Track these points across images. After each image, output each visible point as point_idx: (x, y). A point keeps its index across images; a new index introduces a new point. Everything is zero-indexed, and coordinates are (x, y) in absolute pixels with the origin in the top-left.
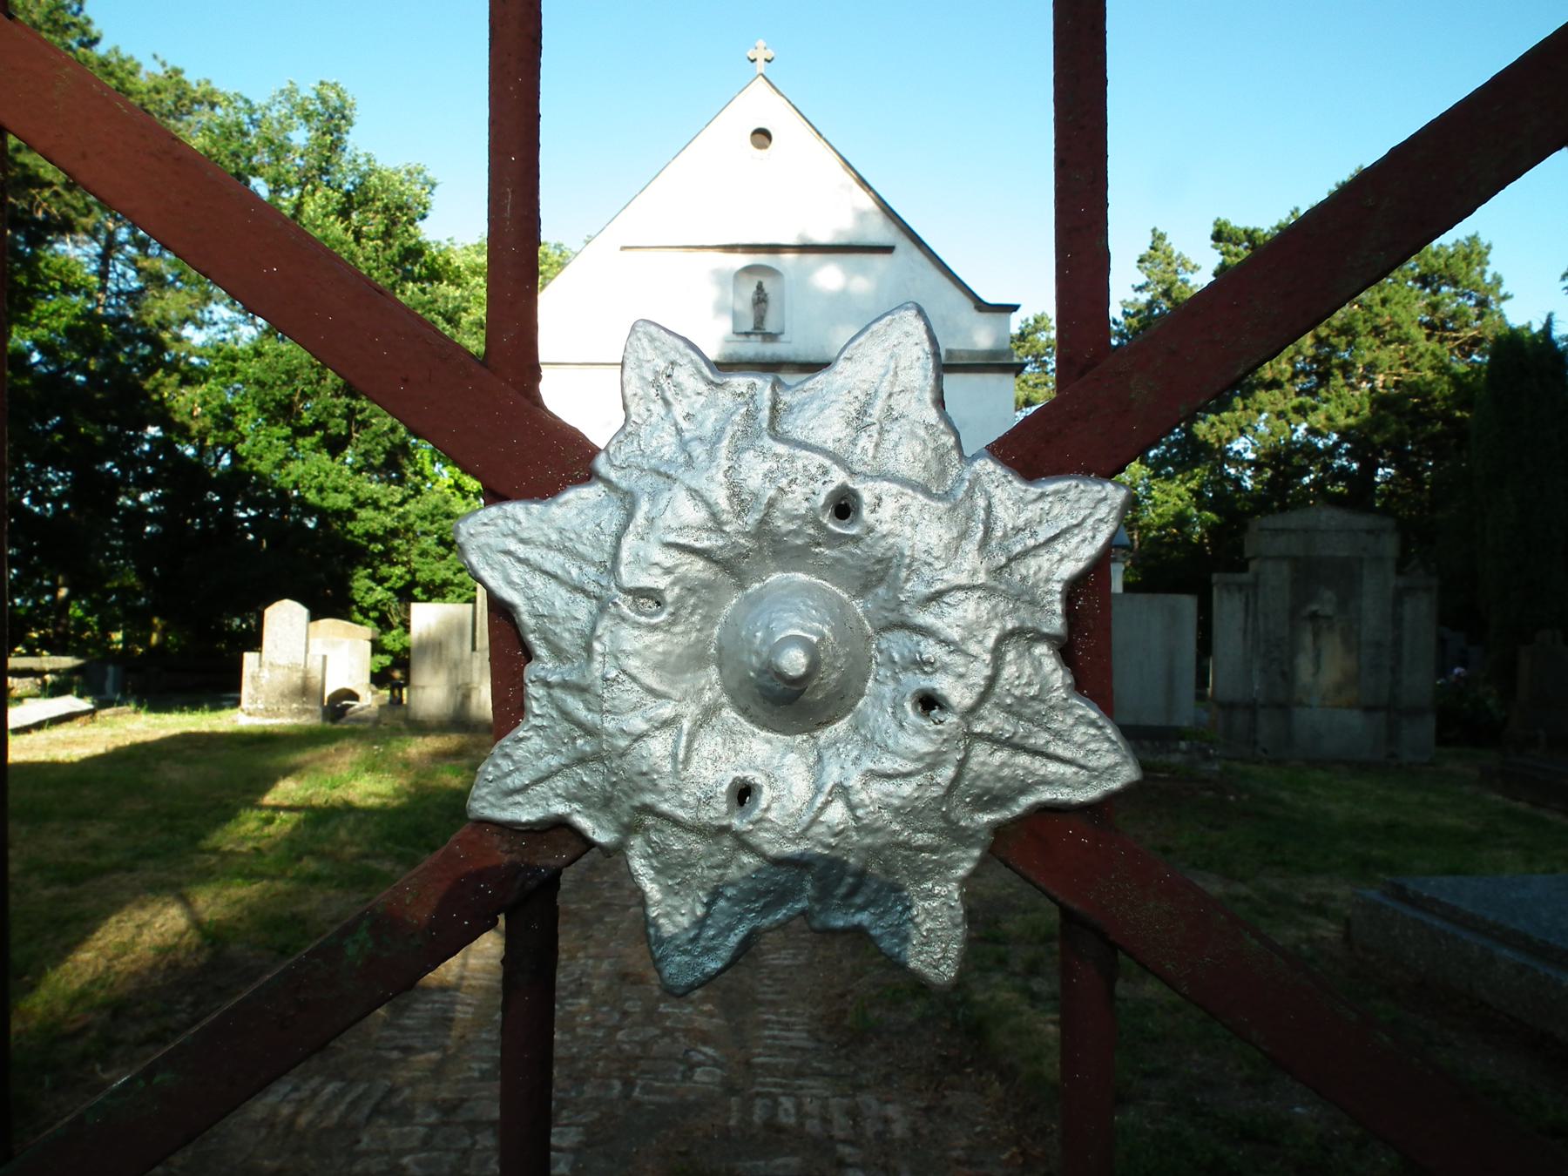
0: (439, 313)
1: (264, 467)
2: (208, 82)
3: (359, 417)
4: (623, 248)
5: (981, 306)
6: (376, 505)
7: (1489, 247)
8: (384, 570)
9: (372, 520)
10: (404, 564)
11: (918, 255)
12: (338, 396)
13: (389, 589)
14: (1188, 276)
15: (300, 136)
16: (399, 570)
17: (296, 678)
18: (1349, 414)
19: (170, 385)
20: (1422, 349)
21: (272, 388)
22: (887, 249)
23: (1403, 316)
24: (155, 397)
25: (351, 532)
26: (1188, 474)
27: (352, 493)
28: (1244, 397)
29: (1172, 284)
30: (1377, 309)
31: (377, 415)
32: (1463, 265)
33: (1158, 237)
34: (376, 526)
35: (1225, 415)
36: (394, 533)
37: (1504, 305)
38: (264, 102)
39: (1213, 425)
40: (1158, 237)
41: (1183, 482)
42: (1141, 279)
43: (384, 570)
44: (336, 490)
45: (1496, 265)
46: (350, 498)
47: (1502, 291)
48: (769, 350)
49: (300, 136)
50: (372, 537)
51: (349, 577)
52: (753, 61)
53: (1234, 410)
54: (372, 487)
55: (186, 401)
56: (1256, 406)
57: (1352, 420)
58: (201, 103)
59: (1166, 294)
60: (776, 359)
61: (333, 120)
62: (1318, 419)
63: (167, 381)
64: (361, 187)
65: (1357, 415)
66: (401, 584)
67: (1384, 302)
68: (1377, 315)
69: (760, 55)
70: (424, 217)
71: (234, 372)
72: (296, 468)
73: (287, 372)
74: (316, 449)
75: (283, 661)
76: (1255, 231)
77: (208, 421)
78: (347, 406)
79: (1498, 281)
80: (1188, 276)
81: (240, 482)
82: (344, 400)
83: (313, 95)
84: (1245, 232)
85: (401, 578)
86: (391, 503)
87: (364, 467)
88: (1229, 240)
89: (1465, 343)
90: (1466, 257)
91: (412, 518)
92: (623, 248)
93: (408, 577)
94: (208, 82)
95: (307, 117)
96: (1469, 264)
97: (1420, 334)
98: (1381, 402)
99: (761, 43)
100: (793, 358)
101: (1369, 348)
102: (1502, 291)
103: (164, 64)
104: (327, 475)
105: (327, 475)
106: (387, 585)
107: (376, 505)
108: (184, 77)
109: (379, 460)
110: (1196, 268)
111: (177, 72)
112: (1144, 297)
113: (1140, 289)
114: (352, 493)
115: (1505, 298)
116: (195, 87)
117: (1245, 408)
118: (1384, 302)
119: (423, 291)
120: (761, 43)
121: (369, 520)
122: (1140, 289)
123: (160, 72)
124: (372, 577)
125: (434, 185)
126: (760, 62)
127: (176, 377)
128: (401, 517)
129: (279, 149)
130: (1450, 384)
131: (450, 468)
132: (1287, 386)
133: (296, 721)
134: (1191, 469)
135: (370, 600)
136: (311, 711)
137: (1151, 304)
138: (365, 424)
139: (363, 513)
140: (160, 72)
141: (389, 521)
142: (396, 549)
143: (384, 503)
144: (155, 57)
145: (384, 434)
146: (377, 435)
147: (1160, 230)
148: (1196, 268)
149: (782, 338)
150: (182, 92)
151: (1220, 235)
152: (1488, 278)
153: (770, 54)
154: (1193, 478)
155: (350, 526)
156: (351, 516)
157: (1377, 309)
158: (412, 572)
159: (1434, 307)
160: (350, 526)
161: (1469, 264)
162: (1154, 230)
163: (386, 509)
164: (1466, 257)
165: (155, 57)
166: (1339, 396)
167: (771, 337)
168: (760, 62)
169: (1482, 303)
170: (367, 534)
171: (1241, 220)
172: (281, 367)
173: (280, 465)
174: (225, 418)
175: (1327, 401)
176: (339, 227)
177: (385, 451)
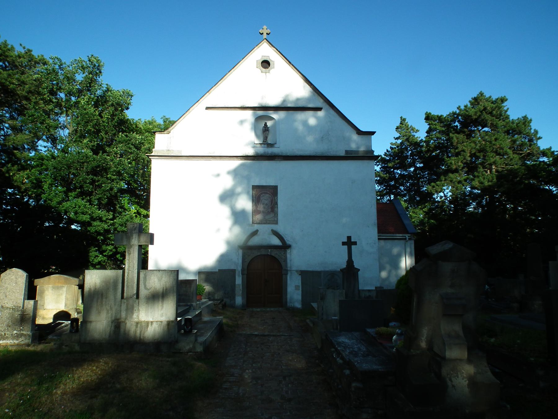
0: (132, 145)
1: (54, 204)
2: (43, 56)
3: (97, 184)
4: (207, 108)
5: (360, 132)
6: (101, 220)
7: (531, 120)
8: (104, 247)
9: (99, 226)
10: (112, 245)
11: (332, 112)
12: (88, 175)
13: (105, 256)
14: (415, 134)
15: (80, 77)
16: (110, 248)
17: (17, 314)
18: (489, 181)
19: (14, 170)
20: (511, 157)
21: (60, 170)
22: (319, 109)
23: (504, 145)
24: (7, 175)
25: (89, 231)
26: (423, 206)
27: (90, 214)
28: (445, 176)
29: (410, 136)
30: (493, 142)
31: (104, 183)
32: (523, 126)
33: (403, 120)
34: (100, 228)
35: (438, 183)
36: (107, 231)
37: (539, 141)
38: (68, 64)
39: (433, 187)
40: (403, 120)
41: (421, 209)
42: (397, 135)
43: (104, 247)
44: (83, 213)
45: (534, 126)
46: (88, 217)
47: (538, 136)
48: (270, 151)
49: (80, 77)
50: (99, 233)
51: (88, 252)
52: (218, 175)
53: (441, 181)
54: (102, 213)
55: (22, 178)
56: (450, 179)
57: (490, 183)
58: (39, 63)
59: (407, 140)
60: (273, 155)
61: (94, 70)
62: (476, 183)
63: (13, 168)
64: (103, 96)
65: (491, 181)
66: (111, 253)
67: (496, 140)
68: (494, 145)
69: (265, 32)
70: (127, 108)
71: (42, 165)
72: (66, 205)
73: (67, 165)
74: (77, 197)
75: (10, 305)
76: (441, 116)
77: (29, 185)
78: (92, 179)
79: (536, 132)
80: (415, 134)
81: (46, 211)
82: (91, 176)
83: (86, 59)
84: (438, 116)
85: (111, 251)
86: (107, 219)
87: (100, 206)
88: (432, 119)
89: (525, 156)
90: (524, 123)
91: (117, 225)
92: (207, 108)
93: (114, 250)
94: (43, 56)
95: (83, 68)
96: (525, 126)
97: (510, 152)
98: (500, 176)
99: (265, 27)
100: (280, 154)
101: (492, 157)
102: (538, 136)
103: (24, 48)
104: (79, 207)
105: (79, 207)
106: (104, 254)
107: (101, 220)
108: (32, 53)
109: (105, 201)
110: (417, 131)
111: (30, 51)
112: (399, 141)
113: (397, 139)
114: (90, 214)
115: (540, 138)
116: (37, 57)
117: (445, 180)
118: (496, 140)
119: (127, 136)
120: (265, 27)
121: (97, 226)
122: (397, 139)
123: (23, 51)
124: (98, 250)
125: (132, 96)
126: (265, 35)
127: (16, 167)
128: (113, 224)
129: (70, 79)
130: (525, 169)
131: (135, 206)
132: (460, 172)
133: (16, 342)
134: (424, 204)
135: (96, 261)
136: (25, 335)
137: (402, 143)
138: (100, 186)
139: (95, 223)
140: (23, 51)
141: (106, 227)
142: (109, 239)
143: (104, 219)
144: (21, 45)
145: (107, 191)
146: (104, 191)
147: (404, 117)
148: (417, 131)
149: (276, 146)
150: (31, 59)
151: (428, 118)
152: (532, 131)
153: (269, 31)
154: (425, 207)
155: (89, 229)
156: (89, 224)
157: (493, 142)
158: (116, 248)
159: (514, 142)
160: (89, 229)
161: (525, 126)
162: (401, 117)
163: (105, 221)
164: (524, 123)
165: (21, 45)
166: (483, 175)
167: (271, 145)
168: (265, 35)
169: (531, 140)
170: (96, 232)
171: (435, 112)
172: (64, 162)
173: (60, 203)
174: (38, 184)
175: (478, 177)
176: (92, 109)
177: (108, 198)
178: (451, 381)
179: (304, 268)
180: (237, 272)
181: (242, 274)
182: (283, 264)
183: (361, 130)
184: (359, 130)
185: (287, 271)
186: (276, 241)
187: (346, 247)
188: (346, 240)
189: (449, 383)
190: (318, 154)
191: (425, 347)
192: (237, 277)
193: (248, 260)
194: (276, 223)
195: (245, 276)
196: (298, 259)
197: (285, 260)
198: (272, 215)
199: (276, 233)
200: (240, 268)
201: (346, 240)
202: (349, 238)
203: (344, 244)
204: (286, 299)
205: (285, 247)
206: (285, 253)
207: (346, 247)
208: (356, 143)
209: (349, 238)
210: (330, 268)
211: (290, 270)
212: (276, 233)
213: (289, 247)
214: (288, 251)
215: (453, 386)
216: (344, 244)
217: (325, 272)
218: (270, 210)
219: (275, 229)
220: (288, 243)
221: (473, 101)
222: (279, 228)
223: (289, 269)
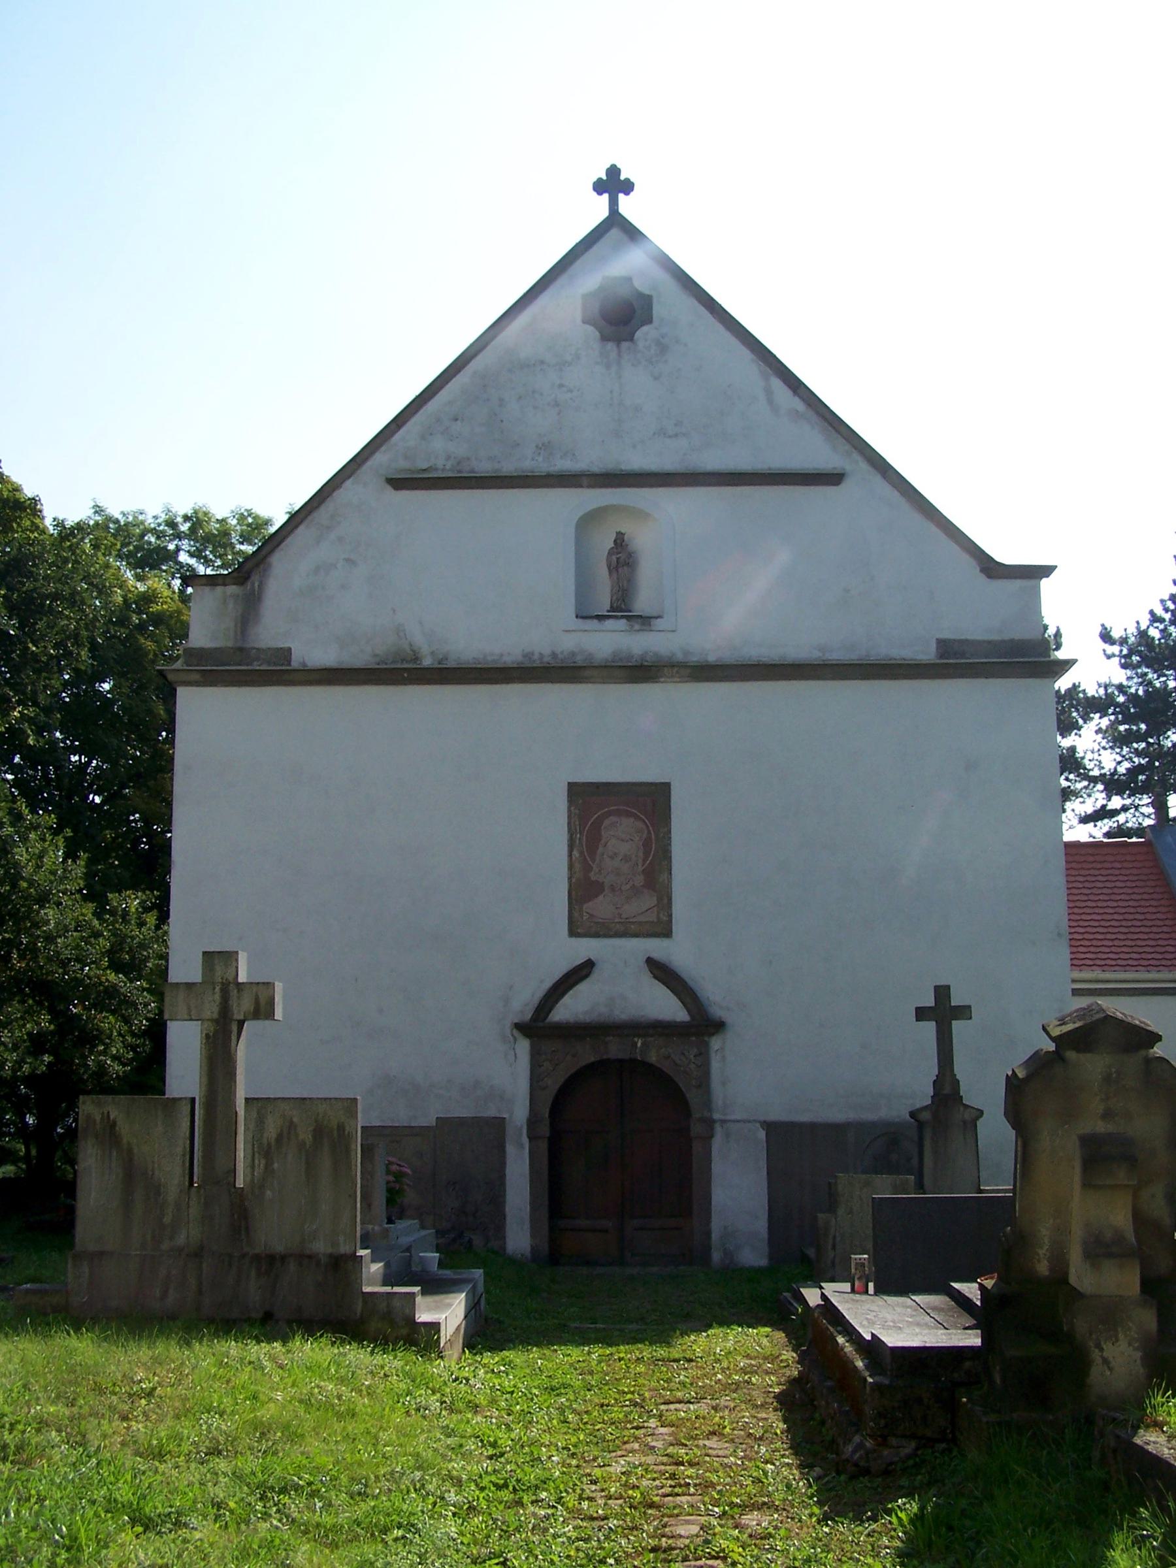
5: (991, 568)
100: (680, 657)
113: (69, 1334)
149: (658, 624)
178: (1102, 1350)
179: (774, 1116)
180: (510, 1131)
181: (531, 1138)
182: (692, 1096)
183: (999, 558)
184: (991, 559)
185: (710, 1123)
186: (664, 1006)
187: (930, 1027)
188: (929, 1001)
189: (1096, 1355)
190: (836, 656)
191: (1047, 1273)
192: (510, 1149)
193: (553, 1084)
194: (667, 933)
195: (544, 1146)
196: (752, 1083)
197: (704, 1082)
198: (649, 900)
199: (661, 971)
200: (519, 1113)
201: (929, 1001)
202: (942, 992)
203: (921, 1014)
204: (708, 1234)
205: (703, 1025)
206: (704, 1055)
207: (930, 1027)
208: (979, 618)
209: (942, 992)
210: (884, 1113)
211: (723, 1122)
212: (661, 971)
213: (718, 1026)
214: (715, 1043)
215: (1106, 1361)
216: (921, 1014)
217: (859, 1127)
218: (639, 880)
219: (656, 955)
220: (717, 1012)
221: (20, 1330)
222: (678, 951)
223: (716, 1116)
